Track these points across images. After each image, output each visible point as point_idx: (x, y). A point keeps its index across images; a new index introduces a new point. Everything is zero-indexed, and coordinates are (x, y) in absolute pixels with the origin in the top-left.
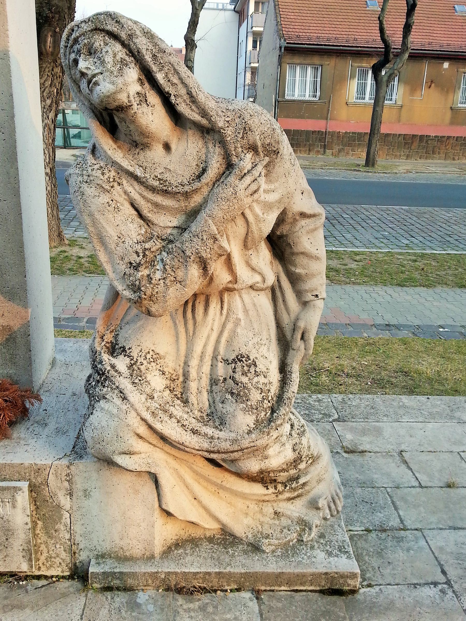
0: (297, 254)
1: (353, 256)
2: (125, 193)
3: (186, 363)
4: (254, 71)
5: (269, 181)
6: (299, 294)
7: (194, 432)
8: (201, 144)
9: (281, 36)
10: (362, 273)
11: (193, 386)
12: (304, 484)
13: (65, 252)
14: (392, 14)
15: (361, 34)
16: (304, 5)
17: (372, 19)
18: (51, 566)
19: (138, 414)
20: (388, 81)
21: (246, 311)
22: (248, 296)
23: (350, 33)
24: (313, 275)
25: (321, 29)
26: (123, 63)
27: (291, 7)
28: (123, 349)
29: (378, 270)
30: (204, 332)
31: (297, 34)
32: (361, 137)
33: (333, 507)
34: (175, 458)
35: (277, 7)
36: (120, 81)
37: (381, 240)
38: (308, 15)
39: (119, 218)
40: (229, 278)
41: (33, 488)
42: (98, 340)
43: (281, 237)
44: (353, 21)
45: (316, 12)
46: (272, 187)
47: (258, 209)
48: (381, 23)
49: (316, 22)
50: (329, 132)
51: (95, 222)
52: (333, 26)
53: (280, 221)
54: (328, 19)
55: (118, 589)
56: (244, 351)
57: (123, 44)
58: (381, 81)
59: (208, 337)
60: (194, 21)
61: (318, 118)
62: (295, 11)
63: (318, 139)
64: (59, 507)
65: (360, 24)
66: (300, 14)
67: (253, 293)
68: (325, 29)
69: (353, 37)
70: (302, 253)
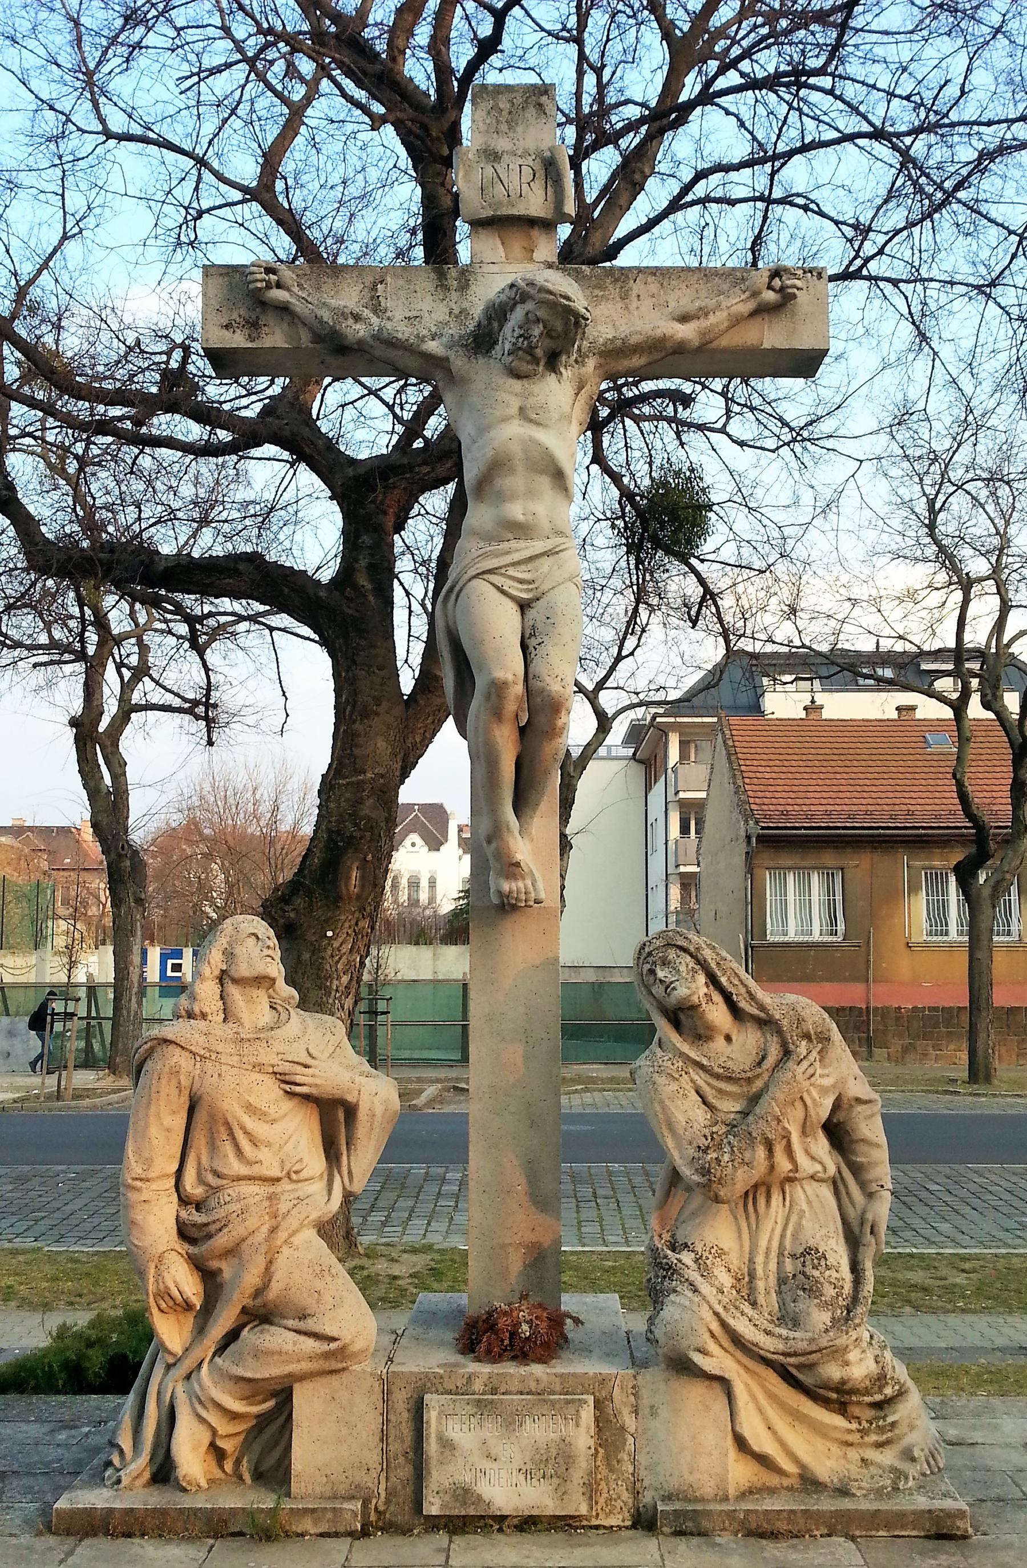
0: (857, 1141)
1: (957, 1262)
2: (692, 1081)
3: (751, 1261)
4: (688, 882)
5: (823, 1066)
6: (863, 1185)
7: (768, 1333)
8: (759, 1034)
9: (748, 815)
10: (980, 1291)
11: (760, 1285)
12: (893, 1424)
13: (363, 1268)
14: (983, 757)
15: (920, 801)
16: (790, 751)
17: (941, 770)
18: (611, 1512)
19: (711, 1307)
20: (995, 897)
21: (809, 1203)
22: (811, 1187)
23: (897, 801)
24: (876, 1164)
25: (833, 795)
26: (694, 971)
27: (765, 757)
28: (686, 1245)
29: (1012, 1286)
30: (767, 1226)
31: (781, 808)
32: (952, 1017)
33: (932, 1462)
34: (747, 1369)
35: (733, 758)
36: (693, 985)
37: (1018, 1233)
38: (802, 770)
39: (687, 1104)
40: (790, 1167)
41: (598, 1404)
42: (656, 1238)
43: (838, 1124)
44: (900, 776)
45: (817, 763)
46: (826, 1071)
47: (815, 1094)
48: (960, 785)
49: (820, 782)
50: (876, 1009)
51: (665, 1109)
52: (858, 788)
53: (837, 1106)
54: (845, 776)
55: (692, 1534)
56: (811, 1243)
57: (691, 955)
58: (979, 895)
59: (773, 1230)
60: (566, 799)
61: (846, 980)
62: (771, 763)
63: (851, 1025)
64: (623, 1429)
65: (916, 782)
66: (784, 769)
67: (815, 1184)
68: (841, 795)
69: (904, 807)
70: (863, 1140)
